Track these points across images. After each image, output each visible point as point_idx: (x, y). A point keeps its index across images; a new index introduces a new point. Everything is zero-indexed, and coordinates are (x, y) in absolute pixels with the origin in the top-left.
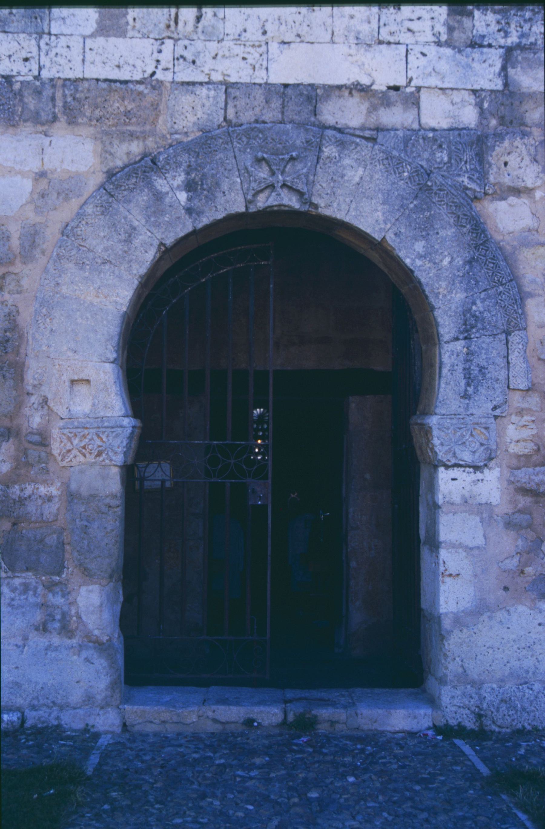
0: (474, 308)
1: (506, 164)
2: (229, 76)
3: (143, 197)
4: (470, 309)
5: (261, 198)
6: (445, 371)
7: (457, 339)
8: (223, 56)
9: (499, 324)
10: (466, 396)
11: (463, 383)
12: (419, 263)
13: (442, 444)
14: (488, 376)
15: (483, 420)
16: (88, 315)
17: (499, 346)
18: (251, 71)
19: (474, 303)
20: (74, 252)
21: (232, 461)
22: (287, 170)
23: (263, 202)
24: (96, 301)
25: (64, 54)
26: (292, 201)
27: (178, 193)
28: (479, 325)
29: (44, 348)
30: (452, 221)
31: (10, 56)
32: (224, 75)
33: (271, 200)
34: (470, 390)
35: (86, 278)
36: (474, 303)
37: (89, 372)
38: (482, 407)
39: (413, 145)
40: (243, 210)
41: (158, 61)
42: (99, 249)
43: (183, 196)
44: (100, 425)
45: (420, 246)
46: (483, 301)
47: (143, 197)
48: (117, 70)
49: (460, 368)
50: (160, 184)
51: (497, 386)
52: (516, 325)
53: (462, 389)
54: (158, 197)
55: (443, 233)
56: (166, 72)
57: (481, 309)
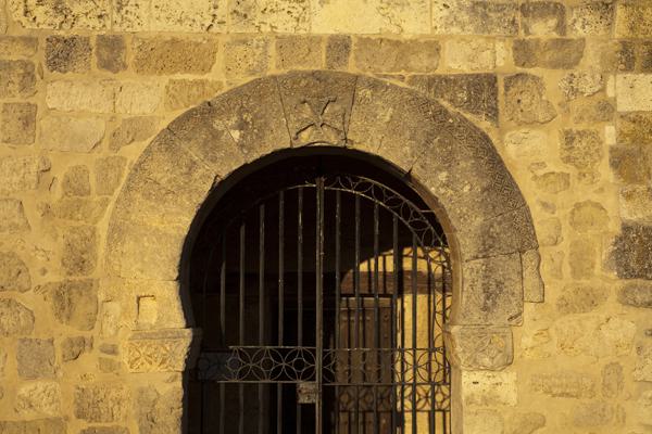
0: (492, 230)
1: (519, 101)
2: (276, 28)
3: (203, 135)
4: (488, 231)
5: (304, 135)
6: (466, 286)
7: (477, 258)
8: (272, 10)
9: (514, 244)
10: (485, 308)
11: (482, 297)
12: (442, 191)
13: (464, 352)
14: (505, 290)
15: (501, 330)
16: (154, 239)
17: (515, 264)
18: (295, 23)
19: (492, 226)
20: (141, 184)
21: (284, 364)
22: (326, 111)
23: (306, 138)
24: (161, 227)
25: (134, 11)
26: (333, 140)
27: (232, 132)
28: (497, 246)
29: (117, 268)
30: (471, 154)
31: (87, 14)
32: (272, 27)
33: (312, 137)
34: (489, 302)
35: (152, 207)
36: (492, 226)
37: (156, 289)
38: (499, 318)
39: (437, 87)
40: (288, 146)
41: (214, 15)
42: (163, 181)
43: (236, 134)
44: (167, 335)
45: (443, 176)
46: (500, 223)
47: (203, 135)
48: (178, 24)
49: (479, 285)
50: (218, 125)
51: (512, 299)
52: (530, 244)
53: (482, 303)
54: (216, 135)
55: (463, 164)
56: (222, 26)
57: (498, 231)
